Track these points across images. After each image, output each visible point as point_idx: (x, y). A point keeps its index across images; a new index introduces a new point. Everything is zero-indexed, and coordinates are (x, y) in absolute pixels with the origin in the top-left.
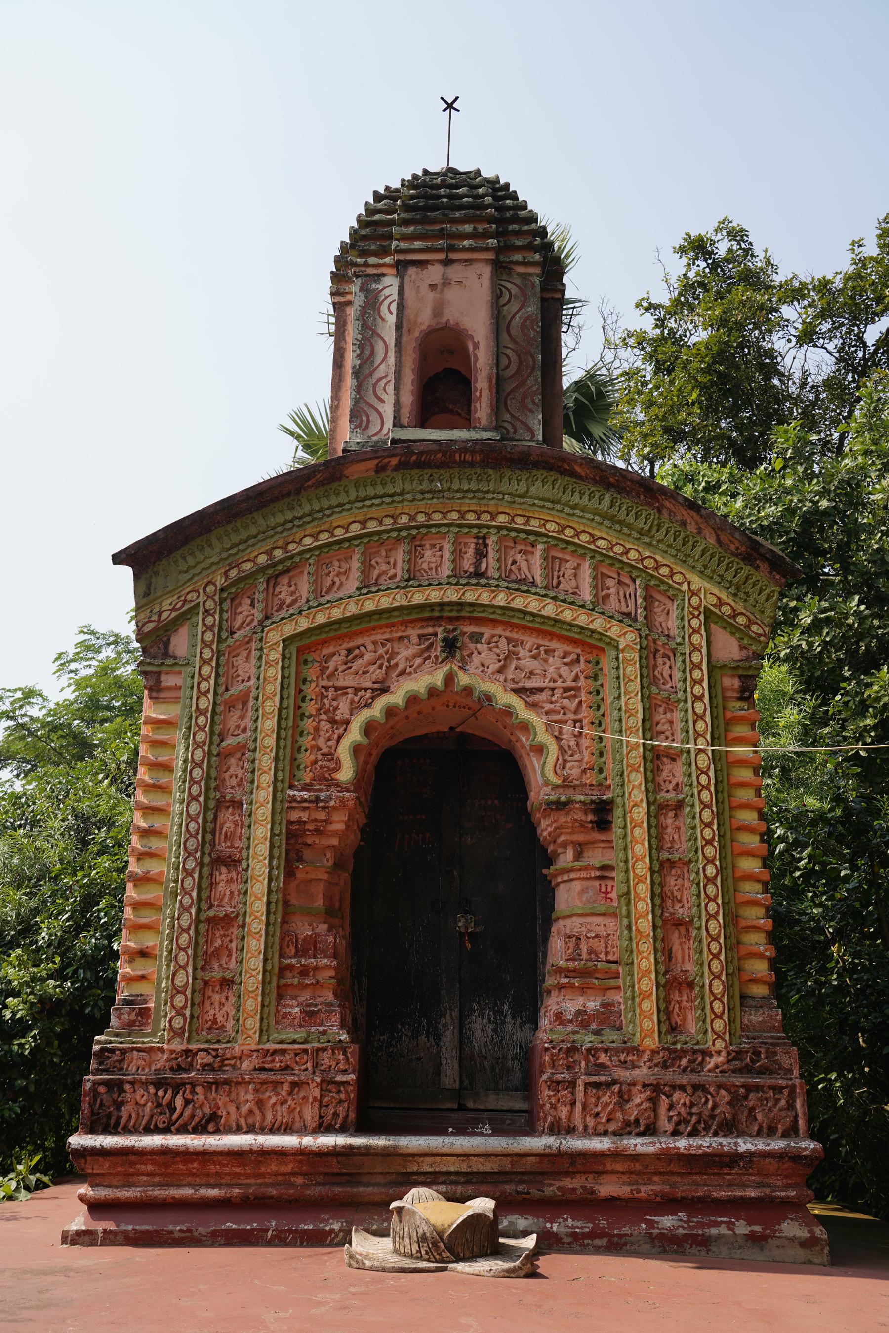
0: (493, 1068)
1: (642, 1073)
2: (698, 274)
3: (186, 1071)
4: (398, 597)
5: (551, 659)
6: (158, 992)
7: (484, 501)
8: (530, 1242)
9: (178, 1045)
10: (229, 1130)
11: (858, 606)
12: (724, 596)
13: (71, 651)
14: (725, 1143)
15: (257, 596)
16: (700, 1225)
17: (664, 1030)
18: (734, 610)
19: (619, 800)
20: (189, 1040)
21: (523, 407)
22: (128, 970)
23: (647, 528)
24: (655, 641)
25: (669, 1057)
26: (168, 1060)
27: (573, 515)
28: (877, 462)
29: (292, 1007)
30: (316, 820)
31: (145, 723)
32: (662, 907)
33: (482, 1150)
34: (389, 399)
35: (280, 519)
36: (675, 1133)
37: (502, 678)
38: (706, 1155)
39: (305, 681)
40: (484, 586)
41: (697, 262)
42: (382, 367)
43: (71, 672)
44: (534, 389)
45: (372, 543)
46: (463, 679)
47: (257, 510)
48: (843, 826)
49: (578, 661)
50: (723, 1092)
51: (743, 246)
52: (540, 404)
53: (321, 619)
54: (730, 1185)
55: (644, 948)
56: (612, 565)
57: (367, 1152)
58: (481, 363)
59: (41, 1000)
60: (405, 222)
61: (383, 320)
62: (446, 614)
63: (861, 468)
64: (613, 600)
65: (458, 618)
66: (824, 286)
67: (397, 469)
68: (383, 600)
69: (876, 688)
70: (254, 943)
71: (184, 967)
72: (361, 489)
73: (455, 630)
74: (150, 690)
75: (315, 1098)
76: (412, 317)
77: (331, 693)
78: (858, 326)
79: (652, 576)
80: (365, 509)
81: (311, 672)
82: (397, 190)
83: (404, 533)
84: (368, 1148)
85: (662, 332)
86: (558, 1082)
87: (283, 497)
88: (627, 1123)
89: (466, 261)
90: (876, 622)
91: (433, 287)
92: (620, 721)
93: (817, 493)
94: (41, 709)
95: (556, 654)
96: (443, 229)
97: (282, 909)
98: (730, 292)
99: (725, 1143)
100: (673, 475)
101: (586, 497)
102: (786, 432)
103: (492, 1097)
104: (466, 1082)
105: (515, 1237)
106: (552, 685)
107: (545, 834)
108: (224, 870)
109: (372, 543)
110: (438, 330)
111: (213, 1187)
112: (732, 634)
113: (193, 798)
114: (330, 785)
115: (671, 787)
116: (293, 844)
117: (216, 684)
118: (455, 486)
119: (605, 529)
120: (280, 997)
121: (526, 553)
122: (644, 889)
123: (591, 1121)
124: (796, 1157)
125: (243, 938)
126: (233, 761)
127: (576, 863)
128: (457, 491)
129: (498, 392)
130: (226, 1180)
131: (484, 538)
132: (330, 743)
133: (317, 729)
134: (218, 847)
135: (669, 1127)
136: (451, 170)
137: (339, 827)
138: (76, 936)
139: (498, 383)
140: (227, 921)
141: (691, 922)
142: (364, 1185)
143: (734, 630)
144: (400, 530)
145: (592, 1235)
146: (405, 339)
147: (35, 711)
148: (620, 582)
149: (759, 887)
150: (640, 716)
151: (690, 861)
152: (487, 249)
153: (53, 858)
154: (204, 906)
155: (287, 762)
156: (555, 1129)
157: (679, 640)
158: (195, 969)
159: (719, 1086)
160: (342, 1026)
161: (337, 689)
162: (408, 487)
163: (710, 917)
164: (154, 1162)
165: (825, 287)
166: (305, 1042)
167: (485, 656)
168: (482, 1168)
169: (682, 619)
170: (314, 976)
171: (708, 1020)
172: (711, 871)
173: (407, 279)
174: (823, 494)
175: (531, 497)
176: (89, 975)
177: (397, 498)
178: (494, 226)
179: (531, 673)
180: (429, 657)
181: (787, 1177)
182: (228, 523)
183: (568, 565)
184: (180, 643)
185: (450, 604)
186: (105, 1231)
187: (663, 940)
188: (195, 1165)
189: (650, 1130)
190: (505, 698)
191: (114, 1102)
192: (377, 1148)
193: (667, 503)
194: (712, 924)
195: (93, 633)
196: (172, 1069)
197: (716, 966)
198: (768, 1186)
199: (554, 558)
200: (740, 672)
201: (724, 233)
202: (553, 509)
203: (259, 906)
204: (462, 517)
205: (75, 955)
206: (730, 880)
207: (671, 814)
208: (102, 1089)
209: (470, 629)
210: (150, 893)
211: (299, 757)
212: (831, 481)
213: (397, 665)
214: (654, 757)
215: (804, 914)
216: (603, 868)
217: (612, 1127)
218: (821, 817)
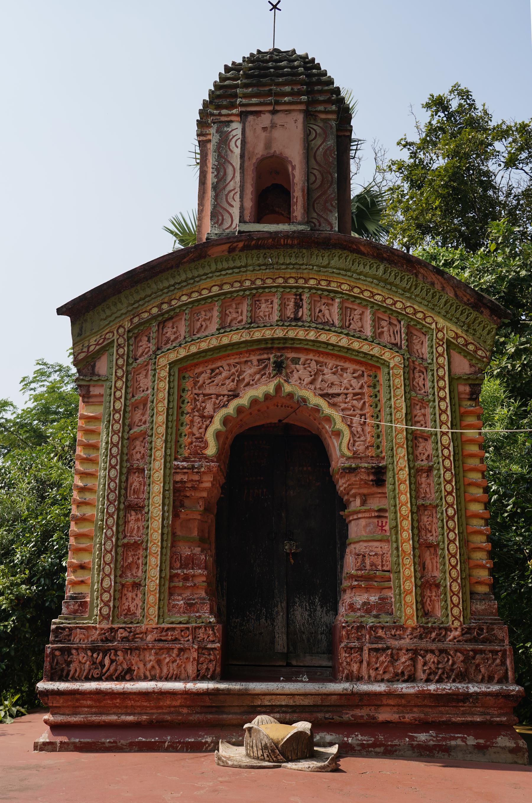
0: (309, 640)
1: (406, 642)
2: (438, 122)
3: (111, 641)
4: (244, 335)
5: (345, 375)
6: (92, 591)
8: (334, 750)
9: (105, 625)
12: (459, 332)
13: (31, 376)
14: (461, 687)
15: (151, 335)
16: (444, 739)
17: (420, 615)
19: (390, 466)
20: (113, 622)
22: (73, 577)
23: (408, 287)
24: (413, 362)
25: (424, 632)
26: (100, 635)
27: (359, 279)
29: (179, 600)
30: (192, 480)
31: (80, 418)
32: (419, 535)
33: (302, 691)
34: (237, 204)
38: (448, 694)
39: (184, 390)
40: (301, 326)
42: (232, 183)
44: (332, 196)
45: (227, 299)
46: (287, 388)
47: (151, 278)
51: (468, 102)
52: (336, 206)
53: (194, 349)
54: (464, 714)
55: (407, 562)
57: (228, 692)
58: (296, 180)
59: (17, 597)
60: (246, 86)
61: (232, 151)
62: (276, 346)
64: (386, 335)
65: (283, 348)
68: (234, 336)
71: (109, 576)
73: (281, 356)
75: (194, 659)
76: (251, 149)
77: (201, 398)
79: (412, 319)
80: (222, 277)
81: (188, 384)
82: (240, 64)
83: (247, 293)
84: (229, 690)
85: (415, 161)
86: (351, 648)
87: (168, 269)
88: (396, 674)
89: (286, 111)
91: (265, 129)
92: (391, 414)
93: (519, 266)
94: (12, 414)
95: (348, 371)
96: (271, 90)
97: (171, 538)
98: (460, 133)
99: (461, 687)
101: (368, 267)
103: (308, 658)
104: (291, 648)
106: (346, 391)
107: (341, 489)
108: (133, 513)
109: (227, 299)
110: (267, 158)
111: (130, 715)
112: (465, 356)
113: (112, 467)
114: (201, 458)
115: (424, 458)
116: (177, 496)
117: (126, 392)
118: (281, 261)
120: (171, 594)
121: (328, 305)
122: (407, 524)
123: (373, 673)
125: (146, 557)
126: (138, 443)
127: (362, 508)
128: (282, 264)
129: (308, 199)
130: (138, 710)
131: (300, 295)
132: (201, 431)
133: (192, 421)
134: (129, 498)
135: (424, 677)
136: (276, 51)
139: (309, 193)
140: (136, 545)
141: (438, 545)
144: (245, 290)
146: (246, 164)
148: (390, 323)
149: (482, 522)
150: (404, 411)
151: (437, 506)
152: (301, 103)
153: (22, 507)
154: (121, 536)
155: (173, 443)
156: (349, 678)
157: (429, 361)
158: (115, 576)
159: (456, 651)
160: (211, 613)
161: (205, 395)
162: (250, 262)
163: (451, 541)
165: (524, 128)
166: (188, 623)
167: (301, 373)
168: (302, 703)
169: (432, 347)
171: (449, 608)
172: (451, 512)
173: (247, 124)
176: (47, 582)
177: (243, 269)
178: (305, 87)
179: (332, 384)
180: (265, 374)
181: (500, 708)
182: (132, 287)
183: (356, 312)
184: (102, 367)
185: (279, 339)
186: (61, 742)
187: (419, 557)
188: (118, 701)
189: (412, 679)
190: (315, 400)
191: (66, 661)
192: (234, 690)
194: (452, 547)
195: (45, 364)
196: (102, 640)
197: (454, 573)
198: (488, 714)
199: (347, 308)
200: (470, 382)
202: (346, 275)
203: (156, 536)
204: (286, 281)
205: (38, 569)
206: (464, 517)
207: (425, 475)
208: (57, 653)
209: (292, 355)
210: (86, 528)
211: (181, 440)
213: (244, 379)
216: (380, 510)
217: (386, 677)
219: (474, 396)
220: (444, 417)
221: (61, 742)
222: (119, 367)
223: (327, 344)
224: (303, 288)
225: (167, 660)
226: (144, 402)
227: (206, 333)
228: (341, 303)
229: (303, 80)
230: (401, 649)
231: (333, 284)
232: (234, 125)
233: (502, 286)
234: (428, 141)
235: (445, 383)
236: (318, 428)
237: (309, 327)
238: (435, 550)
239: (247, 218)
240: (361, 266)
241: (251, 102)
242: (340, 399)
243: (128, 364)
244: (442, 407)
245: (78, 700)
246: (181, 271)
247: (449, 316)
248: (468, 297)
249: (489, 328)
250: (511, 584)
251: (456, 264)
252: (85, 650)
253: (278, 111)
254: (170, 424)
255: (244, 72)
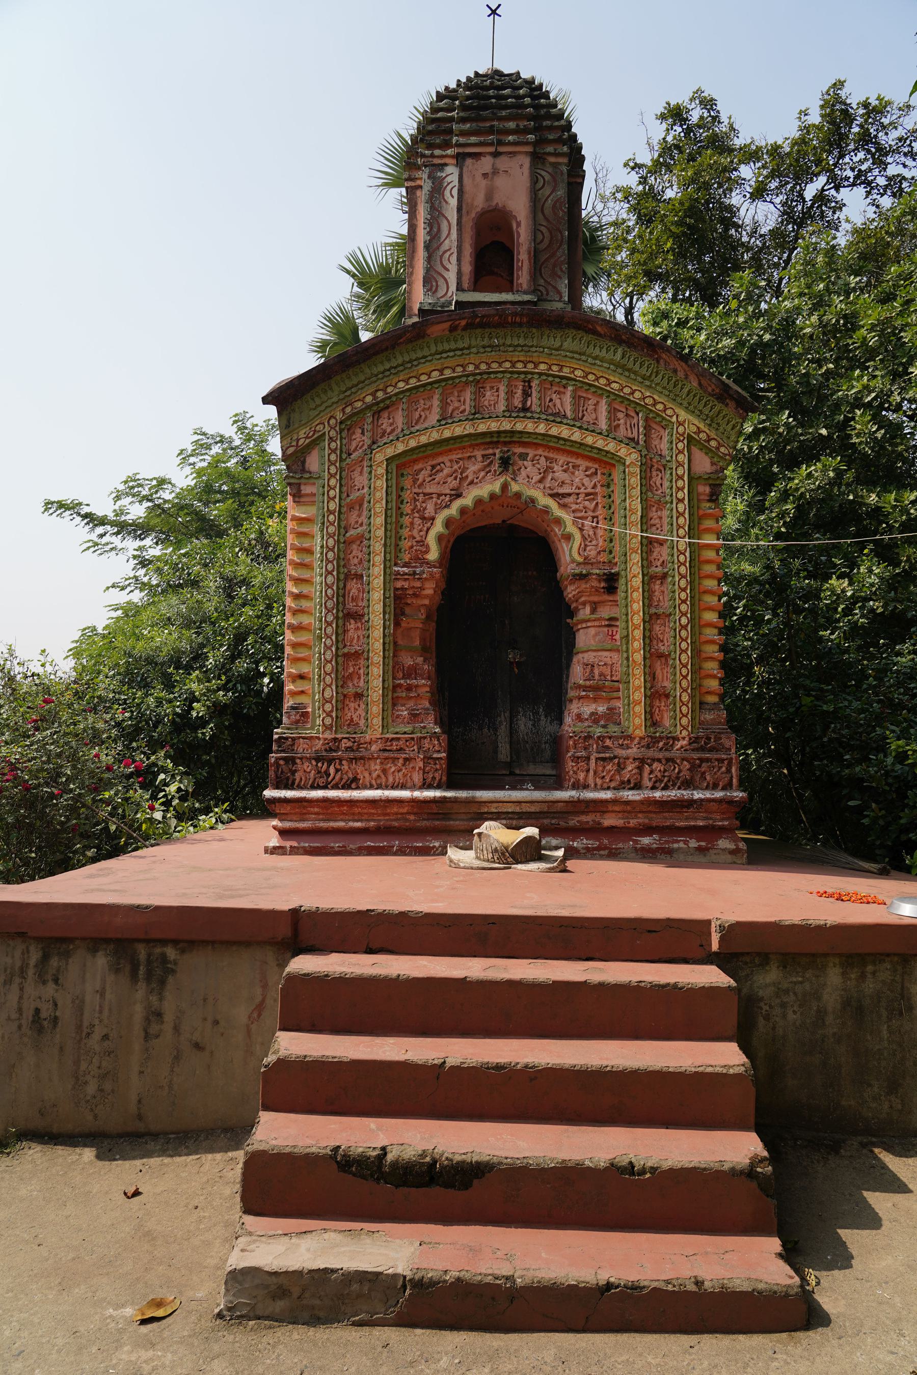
0: (532, 749)
1: (634, 751)
2: (675, 138)
3: (335, 751)
4: (467, 427)
5: (577, 472)
6: (314, 702)
7: (530, 354)
8: (560, 853)
9: (329, 735)
10: (365, 787)
11: (788, 418)
12: (701, 426)
13: (190, 448)
14: (686, 794)
15: (366, 426)
16: (667, 842)
17: (648, 724)
18: (708, 436)
19: (623, 573)
20: (336, 732)
21: (554, 275)
22: (292, 687)
23: (648, 374)
24: (651, 459)
25: (651, 742)
26: (323, 744)
27: (595, 364)
28: (809, 302)
29: (402, 711)
30: (413, 587)
31: (292, 520)
32: (650, 645)
33: (529, 799)
34: (453, 268)
35: (381, 368)
36: (653, 788)
37: (542, 486)
38: (673, 801)
39: (402, 489)
40: (529, 418)
41: (675, 128)
42: (447, 242)
43: (190, 464)
44: (562, 259)
45: (448, 386)
46: (515, 487)
47: (364, 361)
48: (770, 586)
49: (596, 473)
50: (685, 763)
51: (712, 114)
52: (566, 271)
53: (413, 443)
54: (687, 819)
55: (637, 672)
56: (622, 402)
57: (455, 800)
58: (522, 239)
59: (214, 704)
60: (463, 120)
61: (447, 202)
62: (502, 439)
63: (797, 308)
64: (622, 428)
65: (510, 443)
66: (775, 150)
67: (465, 328)
68: (457, 429)
69: (796, 481)
70: (375, 670)
71: (330, 686)
72: (439, 345)
73: (508, 451)
74: (294, 496)
75: (420, 768)
76: (469, 201)
77: (421, 498)
78: (800, 185)
79: (651, 410)
80: (442, 360)
81: (407, 482)
82: (454, 91)
83: (471, 379)
84: (455, 798)
85: (644, 188)
86: (578, 758)
87: (382, 351)
88: (623, 782)
89: (510, 153)
90: (800, 431)
91: (485, 175)
92: (625, 517)
93: (762, 329)
94: (170, 493)
95: (581, 468)
96: (492, 126)
97: (393, 647)
98: (700, 154)
99: (686, 794)
100: (653, 313)
101: (604, 351)
102: (741, 278)
103: (532, 766)
104: (515, 757)
105: (550, 850)
106: (577, 491)
107: (570, 596)
108: (352, 621)
109: (448, 386)
110: (489, 211)
111: (357, 821)
112: (706, 454)
113: (329, 573)
114: (422, 563)
115: (659, 564)
116: (398, 604)
117: (340, 492)
118: (508, 342)
119: (617, 375)
120: (394, 705)
121: (559, 393)
122: (638, 633)
123: (599, 781)
124: (730, 802)
125: (368, 667)
126: (355, 546)
127: (592, 616)
128: (510, 346)
129: (535, 262)
130: (366, 817)
131: (529, 382)
132: (421, 533)
133: (412, 523)
134: (347, 606)
135: (650, 784)
136: (497, 73)
137: (430, 592)
138: (233, 662)
139: (535, 254)
140: (357, 655)
141: (670, 654)
142: (453, 820)
143: (708, 451)
144: (468, 376)
145: (599, 848)
146: (464, 219)
147: (167, 495)
148: (627, 415)
149: (716, 631)
150: (639, 513)
151: (670, 614)
152: (527, 143)
153: (210, 607)
154: (340, 645)
155: (393, 547)
156: (576, 786)
157: (668, 458)
158: (337, 687)
159: (683, 759)
160: (436, 723)
161: (425, 495)
162: (474, 343)
163: (682, 651)
164: (318, 807)
165: (776, 151)
166: (412, 733)
167: (530, 470)
168: (529, 810)
169: (671, 443)
170: (416, 691)
171: (678, 718)
172: (684, 621)
173: (465, 169)
174: (765, 329)
175: (564, 350)
176: (244, 688)
177: (465, 352)
178: (532, 123)
179: (563, 482)
180: (490, 471)
181: (723, 813)
182: (344, 371)
183: (590, 402)
184: (313, 462)
185: (505, 432)
186: (291, 847)
187: (650, 667)
189: (637, 786)
190: (544, 501)
191: (290, 770)
192: (461, 798)
193: (664, 356)
194: (684, 656)
195: (204, 434)
196: (326, 750)
197: (684, 684)
198: (711, 819)
199: (580, 397)
200: (711, 482)
201: (697, 102)
202: (580, 360)
203: (378, 646)
204: (513, 366)
205: (233, 674)
206: (697, 626)
207: (658, 582)
208: (282, 762)
209: (519, 450)
210: (304, 637)
211: (400, 543)
212: (774, 319)
213: (467, 477)
214: (653, 544)
215: (737, 645)
216: (611, 619)
217: (613, 785)
218: (754, 580)
219: (714, 497)
220: (681, 520)
221: (291, 847)
222: (332, 463)
223: (559, 438)
224: (533, 373)
225: (393, 769)
226: (360, 502)
227: (426, 425)
228: (574, 391)
229: (530, 113)
230: (628, 758)
231: (565, 370)
232: (450, 169)
233: (742, 352)
234: (661, 163)
235: (684, 483)
236: (546, 531)
237: (539, 418)
238: (666, 660)
239: (465, 285)
240: (597, 349)
241: (469, 142)
242: (571, 499)
243: (341, 460)
244: (680, 510)
245: (305, 807)
246: (397, 354)
247: (691, 408)
248: (713, 386)
249: (734, 422)
250: (735, 691)
251: (691, 323)
252: (309, 759)
253: (500, 154)
254: (389, 527)
255: (460, 102)
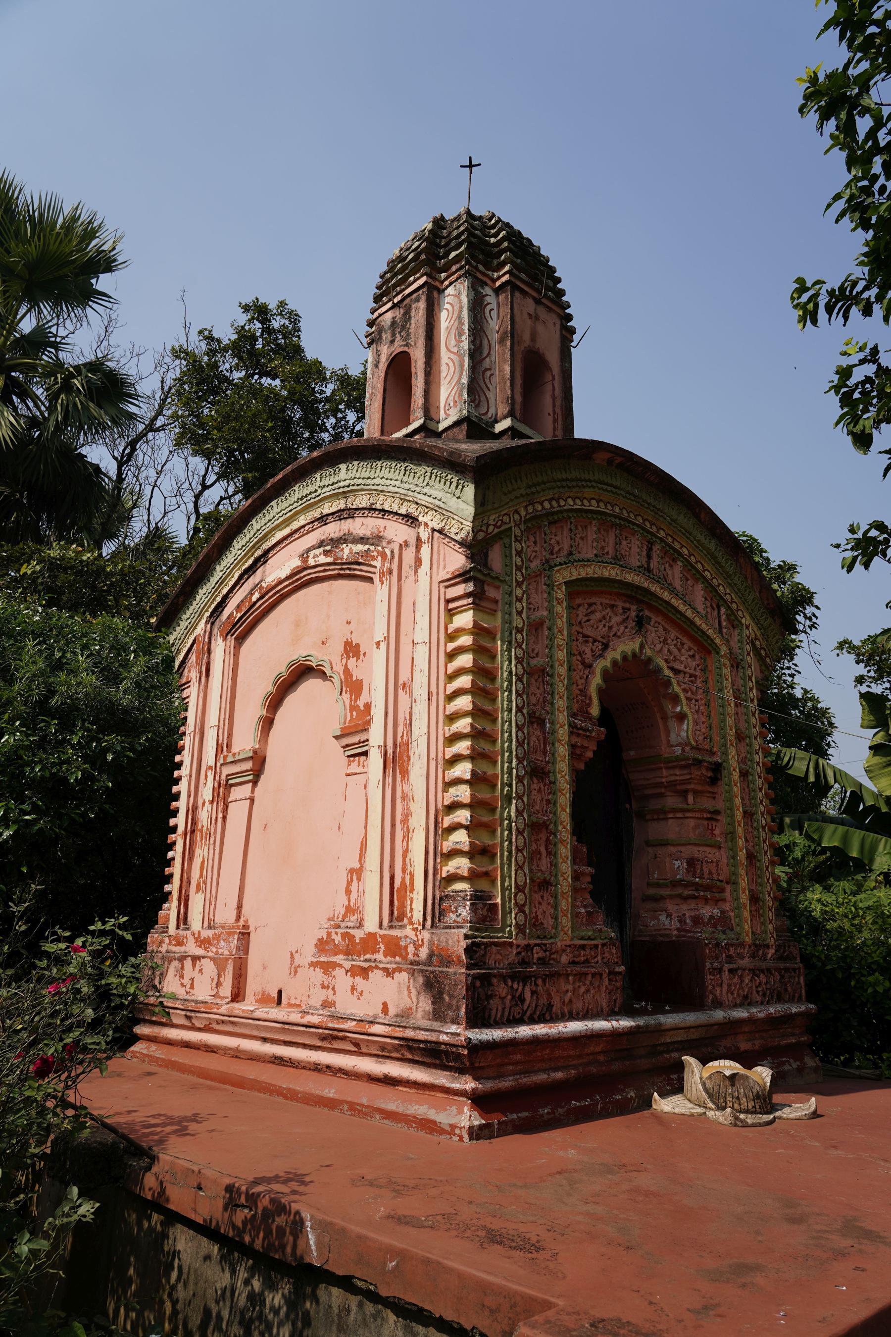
42: (488, 359)
89: (548, 307)
131: (652, 544)
